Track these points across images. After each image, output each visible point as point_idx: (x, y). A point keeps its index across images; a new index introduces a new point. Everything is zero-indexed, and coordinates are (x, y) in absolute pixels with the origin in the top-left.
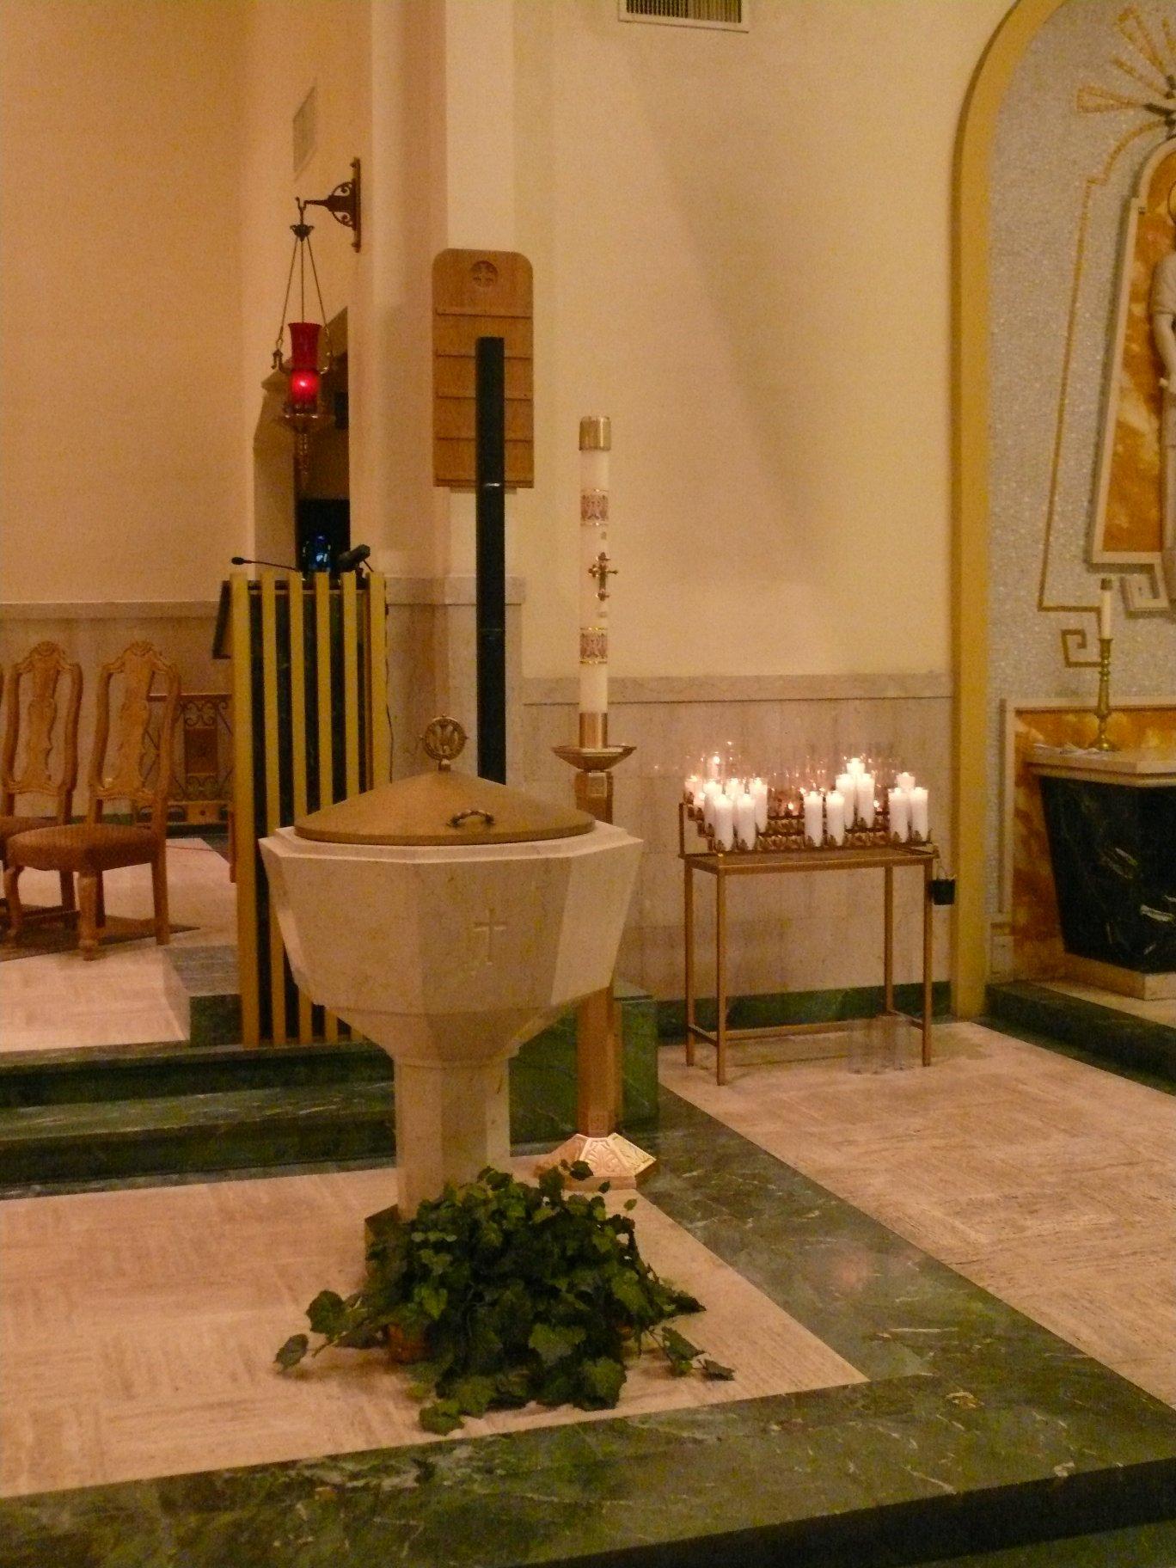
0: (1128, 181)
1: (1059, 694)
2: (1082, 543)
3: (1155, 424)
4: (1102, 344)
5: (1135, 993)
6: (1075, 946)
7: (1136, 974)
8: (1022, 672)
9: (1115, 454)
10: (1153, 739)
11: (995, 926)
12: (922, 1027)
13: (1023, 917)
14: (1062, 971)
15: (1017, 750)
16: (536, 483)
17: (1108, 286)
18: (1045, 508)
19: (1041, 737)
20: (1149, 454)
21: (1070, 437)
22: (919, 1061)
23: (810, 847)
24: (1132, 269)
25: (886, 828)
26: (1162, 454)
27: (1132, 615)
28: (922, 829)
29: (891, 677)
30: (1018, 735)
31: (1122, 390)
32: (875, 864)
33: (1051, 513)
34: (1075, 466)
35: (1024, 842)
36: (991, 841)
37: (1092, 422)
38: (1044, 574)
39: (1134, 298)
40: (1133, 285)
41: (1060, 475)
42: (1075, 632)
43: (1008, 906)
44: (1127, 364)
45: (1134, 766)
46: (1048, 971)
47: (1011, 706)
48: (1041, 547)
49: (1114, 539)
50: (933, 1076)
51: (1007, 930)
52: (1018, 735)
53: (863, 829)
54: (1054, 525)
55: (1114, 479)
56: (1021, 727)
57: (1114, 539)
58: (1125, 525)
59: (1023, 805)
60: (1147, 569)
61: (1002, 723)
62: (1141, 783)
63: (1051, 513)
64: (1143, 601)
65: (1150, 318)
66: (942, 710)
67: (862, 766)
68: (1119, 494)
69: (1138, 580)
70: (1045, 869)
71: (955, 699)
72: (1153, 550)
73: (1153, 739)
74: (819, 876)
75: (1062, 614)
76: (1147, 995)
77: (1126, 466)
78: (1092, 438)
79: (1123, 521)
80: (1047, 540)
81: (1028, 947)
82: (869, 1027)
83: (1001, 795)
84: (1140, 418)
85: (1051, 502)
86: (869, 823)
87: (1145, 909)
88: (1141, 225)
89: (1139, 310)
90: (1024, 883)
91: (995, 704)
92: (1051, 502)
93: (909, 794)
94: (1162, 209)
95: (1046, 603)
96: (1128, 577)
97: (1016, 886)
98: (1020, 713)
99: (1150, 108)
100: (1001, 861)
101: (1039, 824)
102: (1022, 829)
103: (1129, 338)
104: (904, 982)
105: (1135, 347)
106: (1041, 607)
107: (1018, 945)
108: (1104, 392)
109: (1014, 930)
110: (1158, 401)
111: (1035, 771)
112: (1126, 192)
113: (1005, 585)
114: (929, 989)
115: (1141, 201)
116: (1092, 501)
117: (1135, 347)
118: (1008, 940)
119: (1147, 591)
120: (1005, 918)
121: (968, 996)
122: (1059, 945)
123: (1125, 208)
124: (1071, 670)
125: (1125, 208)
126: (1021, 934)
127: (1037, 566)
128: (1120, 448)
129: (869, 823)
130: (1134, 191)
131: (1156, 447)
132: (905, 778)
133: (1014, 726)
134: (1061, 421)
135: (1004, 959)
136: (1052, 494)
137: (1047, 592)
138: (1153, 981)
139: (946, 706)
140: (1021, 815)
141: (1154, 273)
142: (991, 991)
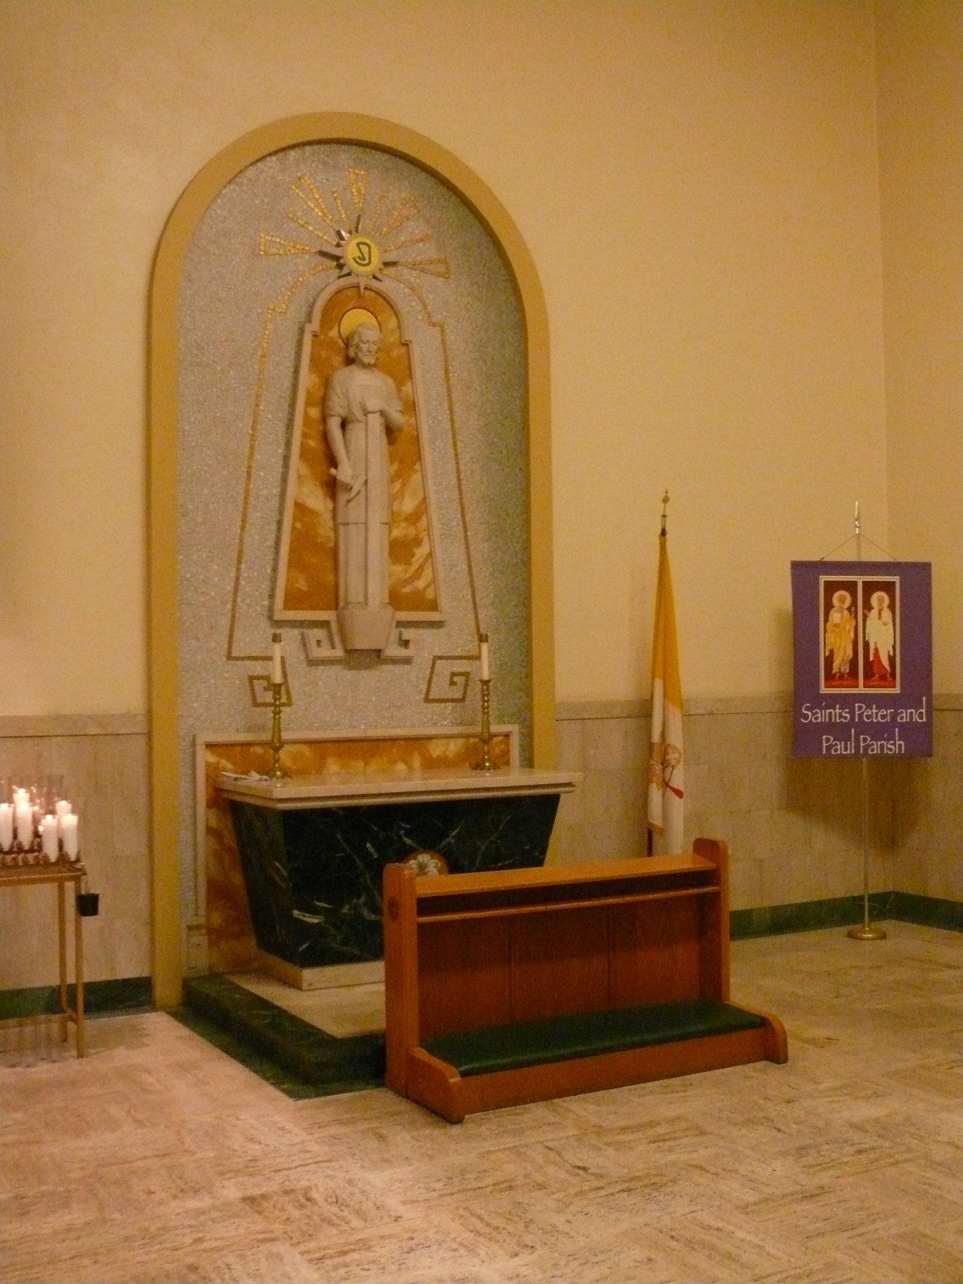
0: (305, 309)
1: (249, 730)
2: (266, 603)
3: (330, 506)
4: (282, 442)
5: (295, 984)
6: (268, 943)
7: (297, 968)
8: (215, 711)
9: (294, 529)
10: (333, 766)
11: (190, 928)
12: (75, 1021)
13: (217, 919)
14: (255, 965)
15: (208, 777)
16: (789, 565)
17: (288, 393)
18: (233, 574)
19: (230, 766)
20: (325, 530)
21: (255, 516)
22: (74, 1053)
23: (47, 863)
24: (308, 380)
25: (40, 849)
26: (336, 530)
27: (313, 663)
28: (72, 850)
29: (90, 717)
30: (208, 765)
31: (299, 477)
32: (49, 880)
33: (237, 579)
34: (259, 539)
35: (218, 856)
36: (188, 855)
37: (274, 503)
38: (232, 630)
39: (309, 403)
40: (309, 392)
41: (245, 547)
42: (262, 678)
43: (202, 912)
44: (304, 455)
45: (271, 792)
46: (241, 966)
47: (200, 740)
48: (229, 606)
49: (294, 600)
50: (87, 1065)
51: (203, 931)
52: (208, 765)
53: (20, 850)
54: (241, 587)
55: (292, 551)
56: (212, 758)
57: (294, 600)
58: (305, 589)
59: (214, 823)
60: (325, 624)
61: (194, 755)
62: (280, 806)
63: (237, 579)
64: (325, 652)
65: (324, 419)
66: (137, 748)
67: (27, 796)
68: (296, 563)
69: (318, 633)
70: (237, 879)
71: (149, 735)
72: (328, 608)
73: (333, 766)
74: (25, 889)
75: (248, 663)
76: (305, 985)
77: (305, 541)
78: (275, 516)
79: (302, 584)
80: (234, 601)
81: (224, 945)
82: (20, 1025)
83: (194, 816)
84: (317, 501)
85: (238, 570)
86: (26, 846)
87: (296, 913)
88: (314, 345)
89: (314, 413)
90: (217, 892)
91: (189, 739)
92: (238, 570)
93: (65, 818)
94: (333, 333)
95: (234, 654)
96: (306, 631)
97: (209, 891)
98: (210, 746)
99: (323, 254)
100: (195, 871)
101: (230, 839)
102: (213, 843)
103: (305, 435)
104: (105, 976)
105: (311, 443)
106: (230, 657)
107: (211, 944)
108: (284, 480)
109: (210, 931)
110: (332, 487)
111: (225, 795)
112: (302, 317)
113: (197, 639)
114: (64, 990)
115: (315, 325)
116: (275, 570)
117: (311, 443)
118: (201, 939)
119: (325, 643)
120: (202, 921)
121: (166, 990)
122: (253, 941)
123: (302, 331)
124: (258, 710)
125: (302, 331)
126: (215, 935)
127: (225, 623)
128: (298, 525)
129: (26, 846)
130: (309, 319)
131: (331, 524)
132: (63, 805)
133: (204, 757)
134: (246, 503)
135: (200, 955)
136: (239, 562)
137: (235, 644)
138: (309, 974)
139: (142, 741)
140: (209, 830)
141: (327, 383)
142: (186, 985)
